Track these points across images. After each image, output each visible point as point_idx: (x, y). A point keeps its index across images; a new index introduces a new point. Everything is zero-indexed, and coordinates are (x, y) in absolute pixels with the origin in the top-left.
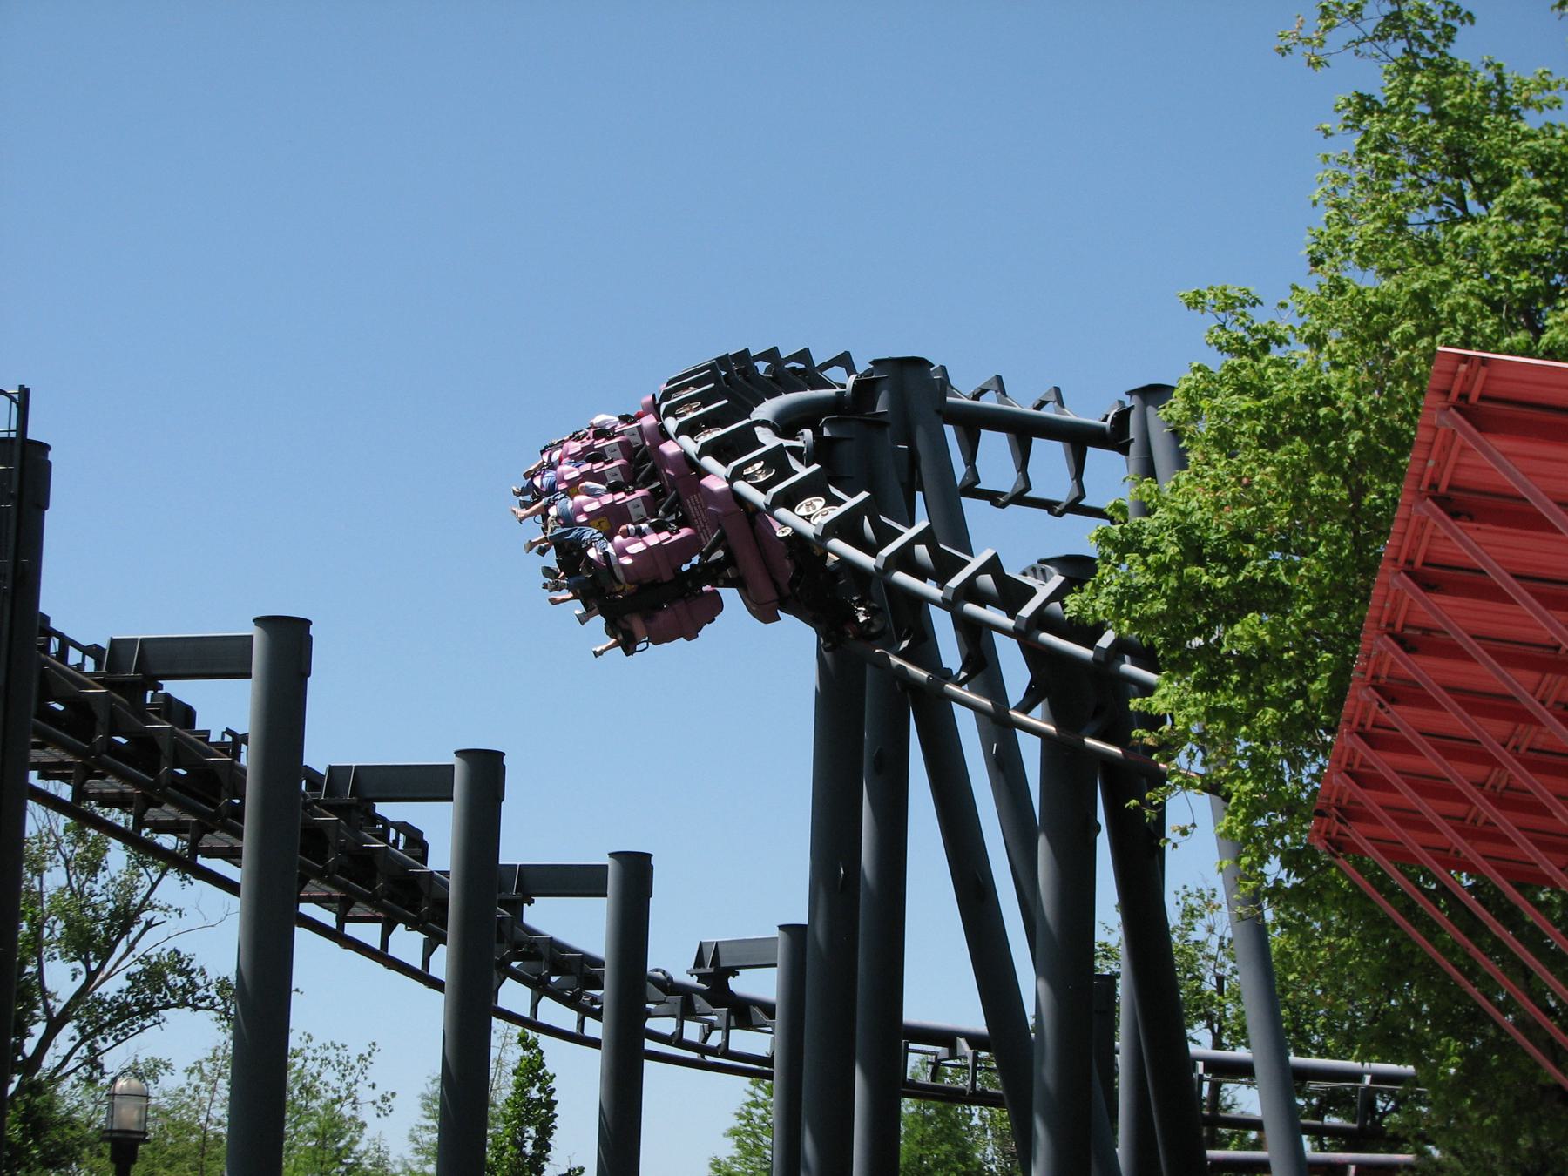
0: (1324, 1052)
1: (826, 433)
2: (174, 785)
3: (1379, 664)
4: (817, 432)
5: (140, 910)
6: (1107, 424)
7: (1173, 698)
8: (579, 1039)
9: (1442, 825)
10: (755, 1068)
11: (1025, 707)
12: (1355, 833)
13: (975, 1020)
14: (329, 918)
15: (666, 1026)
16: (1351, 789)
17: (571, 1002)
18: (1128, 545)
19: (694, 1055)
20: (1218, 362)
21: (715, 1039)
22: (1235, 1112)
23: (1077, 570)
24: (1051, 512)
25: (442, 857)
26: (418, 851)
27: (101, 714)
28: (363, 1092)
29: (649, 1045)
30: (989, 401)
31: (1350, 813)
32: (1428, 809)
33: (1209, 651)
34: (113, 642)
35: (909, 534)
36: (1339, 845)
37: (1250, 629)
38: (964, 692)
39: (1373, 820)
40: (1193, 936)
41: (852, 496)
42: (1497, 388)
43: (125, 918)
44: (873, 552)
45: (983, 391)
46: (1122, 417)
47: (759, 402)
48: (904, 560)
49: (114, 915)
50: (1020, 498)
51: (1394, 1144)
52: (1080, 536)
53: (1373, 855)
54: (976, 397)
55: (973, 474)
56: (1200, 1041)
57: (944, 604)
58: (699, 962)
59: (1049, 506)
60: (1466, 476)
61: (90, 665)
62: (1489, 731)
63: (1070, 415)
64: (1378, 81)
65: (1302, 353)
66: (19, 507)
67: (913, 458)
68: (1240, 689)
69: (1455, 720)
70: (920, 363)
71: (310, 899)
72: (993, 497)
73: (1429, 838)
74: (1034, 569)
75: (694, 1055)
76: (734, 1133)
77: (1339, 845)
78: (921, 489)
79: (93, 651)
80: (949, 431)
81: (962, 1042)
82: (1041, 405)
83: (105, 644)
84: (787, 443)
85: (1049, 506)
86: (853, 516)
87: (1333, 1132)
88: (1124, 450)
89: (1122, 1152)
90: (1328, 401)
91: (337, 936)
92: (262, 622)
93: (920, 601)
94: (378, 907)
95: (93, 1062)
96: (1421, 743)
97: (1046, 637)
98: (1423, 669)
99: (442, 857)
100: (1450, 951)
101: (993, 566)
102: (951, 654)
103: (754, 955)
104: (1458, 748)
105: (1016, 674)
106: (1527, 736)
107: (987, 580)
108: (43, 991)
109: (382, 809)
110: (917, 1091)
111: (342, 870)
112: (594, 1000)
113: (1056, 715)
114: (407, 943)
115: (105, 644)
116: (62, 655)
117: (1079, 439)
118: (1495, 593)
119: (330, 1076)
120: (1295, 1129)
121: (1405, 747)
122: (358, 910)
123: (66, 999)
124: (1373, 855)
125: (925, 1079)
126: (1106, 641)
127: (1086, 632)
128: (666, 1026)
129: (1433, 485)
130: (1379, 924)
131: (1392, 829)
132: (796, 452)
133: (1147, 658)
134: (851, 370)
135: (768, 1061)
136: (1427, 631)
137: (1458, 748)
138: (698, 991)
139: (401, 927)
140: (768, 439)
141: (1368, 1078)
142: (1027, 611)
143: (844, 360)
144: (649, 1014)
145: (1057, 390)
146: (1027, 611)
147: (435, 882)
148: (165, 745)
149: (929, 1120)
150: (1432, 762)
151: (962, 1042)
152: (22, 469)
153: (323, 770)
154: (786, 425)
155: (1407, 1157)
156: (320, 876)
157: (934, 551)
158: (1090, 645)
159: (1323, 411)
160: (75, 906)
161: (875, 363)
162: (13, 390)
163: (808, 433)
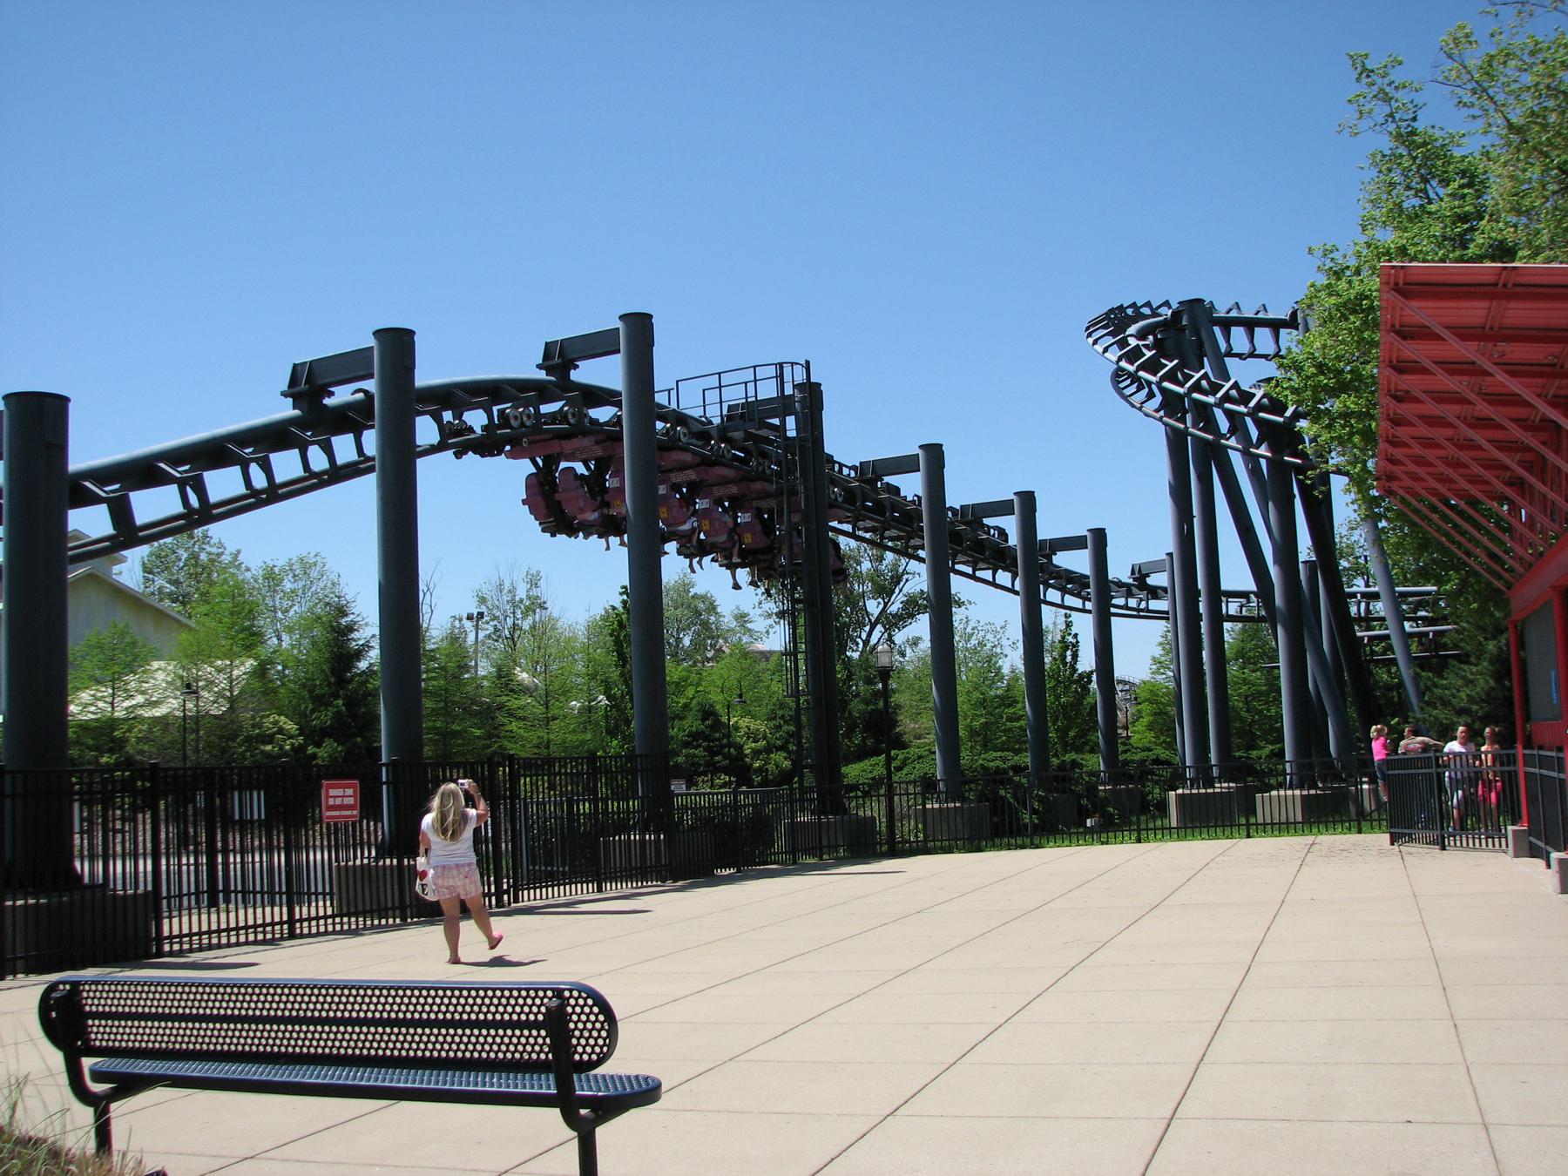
1: (1159, 336)
2: (893, 520)
3: (1388, 409)
4: (1155, 336)
5: (903, 574)
6: (1288, 318)
8: (1084, 610)
9: (1428, 478)
12: (1394, 486)
13: (1251, 585)
14: (969, 570)
15: (1120, 601)
17: (1078, 595)
19: (1135, 613)
20: (1322, 280)
21: (1143, 605)
24: (1241, 359)
25: (1013, 540)
26: (1004, 538)
27: (859, 494)
28: (1004, 642)
29: (1113, 610)
30: (1234, 314)
32: (1420, 471)
34: (861, 463)
40: (1353, 539)
41: (1171, 361)
42: (1411, 279)
43: (897, 579)
44: (1182, 386)
45: (1231, 310)
46: (1294, 314)
48: (1197, 387)
49: (892, 577)
50: (1252, 355)
54: (1228, 313)
57: (1248, 414)
58: (1133, 572)
59: (1265, 357)
60: (1406, 320)
61: (853, 474)
63: (1271, 316)
64: (1386, 144)
66: (811, 411)
67: (1200, 344)
69: (1423, 430)
70: (1200, 301)
71: (959, 563)
72: (1240, 356)
74: (1255, 385)
75: (1135, 613)
76: (1160, 644)
79: (853, 468)
80: (1217, 330)
81: (1252, 596)
82: (1257, 313)
83: (858, 465)
84: (1141, 343)
85: (1265, 357)
87: (1422, 618)
91: (973, 577)
92: (377, 334)
94: (988, 563)
95: (890, 639)
98: (1405, 410)
99: (1013, 540)
102: (1224, 424)
103: (1157, 567)
104: (1428, 443)
107: (1234, 392)
108: (867, 612)
109: (986, 521)
111: (970, 548)
112: (1089, 593)
113: (1271, 448)
114: (1004, 577)
115: (858, 465)
116: (840, 471)
117: (1276, 326)
119: (989, 636)
120: (1401, 618)
121: (1438, 446)
122: (981, 565)
123: (875, 616)
126: (1288, 414)
127: (1277, 407)
128: (1120, 601)
129: (1393, 326)
130: (1412, 525)
131: (1409, 483)
132: (1146, 346)
134: (1170, 307)
135: (1167, 613)
136: (1407, 392)
137: (1428, 443)
138: (1133, 585)
139: (1000, 571)
140: (1133, 342)
142: (1252, 404)
144: (1113, 597)
145: (1264, 305)
146: (1252, 404)
147: (1012, 550)
148: (887, 504)
150: (1418, 450)
151: (1252, 596)
152: (810, 395)
153: (958, 508)
154: (1141, 335)
156: (960, 552)
158: (1282, 416)
160: (875, 575)
161: (1179, 303)
162: (803, 362)
163: (1151, 338)
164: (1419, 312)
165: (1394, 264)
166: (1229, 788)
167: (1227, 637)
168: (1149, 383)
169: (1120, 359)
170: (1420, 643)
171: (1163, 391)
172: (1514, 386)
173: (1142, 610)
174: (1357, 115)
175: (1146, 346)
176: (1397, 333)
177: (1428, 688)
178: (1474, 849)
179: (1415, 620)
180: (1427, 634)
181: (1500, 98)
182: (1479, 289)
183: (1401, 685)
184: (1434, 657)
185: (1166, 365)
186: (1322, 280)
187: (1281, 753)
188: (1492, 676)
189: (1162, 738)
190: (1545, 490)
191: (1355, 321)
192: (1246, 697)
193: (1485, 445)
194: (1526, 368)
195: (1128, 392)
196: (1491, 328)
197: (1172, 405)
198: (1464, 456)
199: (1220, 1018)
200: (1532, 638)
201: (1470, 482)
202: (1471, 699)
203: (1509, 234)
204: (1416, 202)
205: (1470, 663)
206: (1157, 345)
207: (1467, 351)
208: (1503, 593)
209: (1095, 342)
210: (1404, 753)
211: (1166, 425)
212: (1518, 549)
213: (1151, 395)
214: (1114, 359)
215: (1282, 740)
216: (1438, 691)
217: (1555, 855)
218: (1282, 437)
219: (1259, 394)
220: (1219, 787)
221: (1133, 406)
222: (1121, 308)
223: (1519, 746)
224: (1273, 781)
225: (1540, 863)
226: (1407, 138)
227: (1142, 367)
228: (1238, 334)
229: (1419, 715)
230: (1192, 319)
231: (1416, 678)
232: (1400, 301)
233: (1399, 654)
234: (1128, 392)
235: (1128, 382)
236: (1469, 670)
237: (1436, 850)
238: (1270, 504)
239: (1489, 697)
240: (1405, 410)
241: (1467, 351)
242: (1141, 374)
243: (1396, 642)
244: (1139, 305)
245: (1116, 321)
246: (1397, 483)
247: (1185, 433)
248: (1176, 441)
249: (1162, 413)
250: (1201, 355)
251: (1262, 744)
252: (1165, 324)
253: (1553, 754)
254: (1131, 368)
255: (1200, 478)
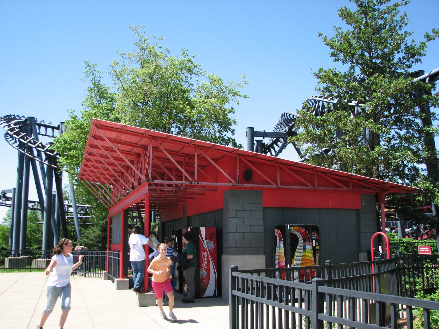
0: (81, 204)
1: (21, 125)
4: (19, 125)
7: (63, 160)
9: (94, 177)
10: (9, 206)
11: (45, 161)
12: (83, 177)
13: (38, 200)
16: (83, 172)
18: (57, 142)
20: (70, 119)
22: (70, 211)
23: (51, 144)
30: (42, 123)
31: (83, 175)
32: (92, 174)
33: (67, 155)
35: (30, 139)
36: (82, 179)
37: (72, 152)
38: (37, 159)
39: (85, 176)
40: (66, 190)
42: (100, 124)
44: (25, 140)
45: (41, 122)
46: (59, 126)
47: (12, 121)
48: (30, 142)
50: (46, 135)
51: (89, 215)
52: (52, 140)
53: (85, 180)
55: (40, 131)
56: (66, 203)
57: (35, 148)
58: (2, 192)
59: (49, 136)
60: (96, 134)
62: (99, 165)
63: (53, 125)
65: (81, 119)
67: (32, 130)
68: (71, 159)
69: (95, 164)
70: (33, 118)
72: (42, 135)
73: (92, 178)
76: (7, 214)
77: (82, 179)
78: (382, 245)
82: (49, 124)
85: (49, 136)
86: (24, 136)
87: (82, 214)
88: (59, 130)
89: (56, 216)
90: (83, 125)
93: (31, 148)
96: (91, 166)
97: (48, 152)
98: (91, 158)
100: (95, 192)
101: (41, 143)
102: (36, 154)
103: (9, 191)
104: (95, 167)
105: (44, 157)
106: (104, 166)
107: (40, 145)
110: (30, 209)
113: (49, 162)
117: (53, 128)
118: (100, 149)
120: (77, 213)
124: (85, 180)
125: (31, 207)
126: (55, 153)
127: (52, 151)
129: (92, 135)
131: (88, 177)
132: (16, 128)
133: (60, 155)
135: (10, 205)
136: (92, 153)
137: (95, 167)
140: (13, 126)
141: (86, 207)
142: (45, 149)
143: (24, 117)
146: (45, 149)
149: (32, 212)
150: (92, 169)
154: (15, 124)
155: (90, 216)
157: (34, 141)
159: (83, 126)
164: (100, 133)
165: (97, 119)
166: (24, 257)
167: (28, 213)
168: (16, 138)
169: (8, 130)
170: (81, 220)
171: (20, 141)
172: (122, 156)
173: (3, 204)
174: (86, 77)
175: (16, 128)
176: (93, 137)
177: (83, 233)
178: (93, 277)
179: (81, 213)
180: (83, 218)
181: (122, 81)
182: (116, 129)
183: (75, 231)
184: (85, 224)
185: (21, 134)
186: (70, 119)
187: (40, 248)
188: (100, 230)
189: (4, 242)
190: (123, 182)
191: (79, 131)
192: (31, 231)
193: (111, 170)
194: (126, 152)
195: (9, 140)
196: (117, 140)
197: (21, 146)
198: (105, 172)
199: (27, 325)
200: (114, 222)
201: (105, 179)
202: (94, 236)
203: (119, 116)
204: (97, 102)
205: (94, 227)
206: (20, 128)
207: (110, 144)
208: (107, 209)
209: (1, 124)
210: (77, 250)
211: (19, 151)
212: (114, 198)
213: (16, 142)
214: (7, 130)
215: (41, 244)
216: (86, 234)
217: (116, 280)
218: (52, 159)
219: (47, 146)
220: (22, 257)
221: (10, 144)
222: (10, 116)
223: (107, 250)
224: (37, 256)
225: (110, 281)
226: (97, 85)
227: (14, 134)
228: (43, 129)
229: (80, 240)
230: (31, 122)
231: (80, 230)
232: (96, 129)
233: (76, 223)
234: (9, 140)
235: (9, 137)
236: (94, 229)
237: (83, 277)
238: (46, 178)
239: (99, 237)
240: (91, 158)
241: (110, 144)
242: (14, 135)
243: (75, 219)
244: (16, 115)
245: (8, 119)
246: (85, 177)
247: (24, 154)
248: (21, 157)
249: (18, 147)
250: (32, 132)
251: (34, 245)
252: (22, 122)
253: (117, 253)
254: (11, 133)
255: (26, 167)
